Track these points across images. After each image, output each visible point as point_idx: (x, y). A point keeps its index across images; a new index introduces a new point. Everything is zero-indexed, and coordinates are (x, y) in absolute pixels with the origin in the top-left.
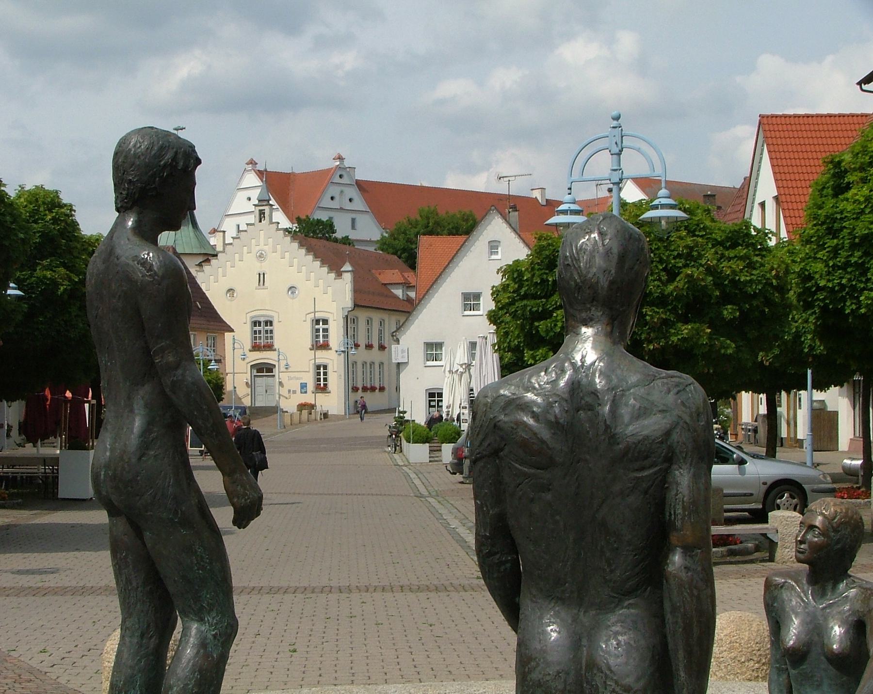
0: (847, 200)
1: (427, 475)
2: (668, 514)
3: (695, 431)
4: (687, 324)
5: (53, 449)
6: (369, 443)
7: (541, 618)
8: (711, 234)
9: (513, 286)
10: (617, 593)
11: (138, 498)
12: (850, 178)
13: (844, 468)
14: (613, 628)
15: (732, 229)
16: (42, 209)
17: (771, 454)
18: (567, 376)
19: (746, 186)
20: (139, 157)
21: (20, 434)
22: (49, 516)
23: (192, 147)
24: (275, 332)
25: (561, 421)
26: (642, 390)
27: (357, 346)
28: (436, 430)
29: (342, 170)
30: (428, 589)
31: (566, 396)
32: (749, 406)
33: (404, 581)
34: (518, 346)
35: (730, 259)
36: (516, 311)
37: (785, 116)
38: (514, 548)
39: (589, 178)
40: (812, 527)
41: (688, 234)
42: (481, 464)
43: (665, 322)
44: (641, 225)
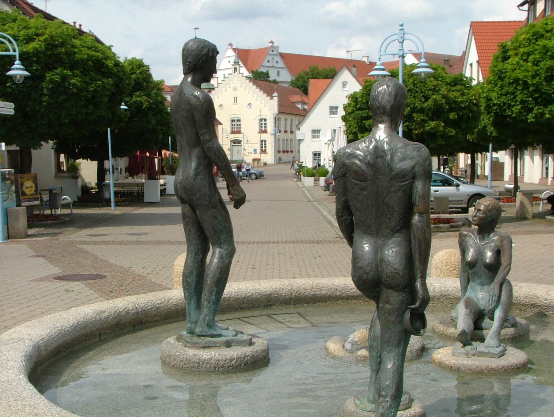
0: (508, 63)
5: (142, 179)
6: (286, 177)
7: (362, 242)
12: (510, 53)
13: (506, 188)
17: (472, 182)
23: (215, 46)
27: (280, 131)
28: (317, 171)
29: (273, 48)
30: (314, 242)
31: (372, 152)
32: (463, 160)
33: (303, 239)
34: (355, 132)
35: (453, 91)
37: (483, 22)
38: (351, 214)
39: (389, 53)
40: (479, 210)
42: (338, 179)
43: (423, 120)
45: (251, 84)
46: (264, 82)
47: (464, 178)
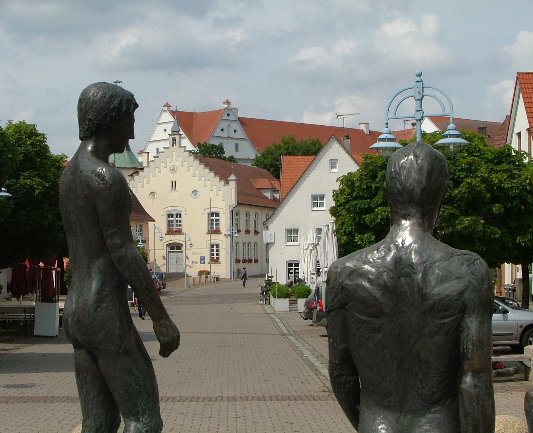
1: (288, 321)
2: (462, 349)
3: (480, 291)
4: (467, 216)
7: (374, 420)
8: (484, 154)
9: (348, 190)
10: (428, 403)
11: (94, 336)
14: (424, 427)
15: (499, 151)
16: (24, 137)
17: (525, 306)
18: (392, 254)
19: (508, 122)
20: (96, 103)
21: (8, 291)
22: (28, 348)
23: (132, 96)
24: (183, 222)
25: (388, 284)
26: (444, 263)
27: (239, 231)
29: (229, 111)
33: (273, 393)
35: (497, 172)
36: (350, 208)
38: (355, 372)
41: (468, 154)
42: (333, 314)
43: (452, 215)
44: (438, 147)
45: (197, 162)
46: (216, 160)
47: (513, 301)
